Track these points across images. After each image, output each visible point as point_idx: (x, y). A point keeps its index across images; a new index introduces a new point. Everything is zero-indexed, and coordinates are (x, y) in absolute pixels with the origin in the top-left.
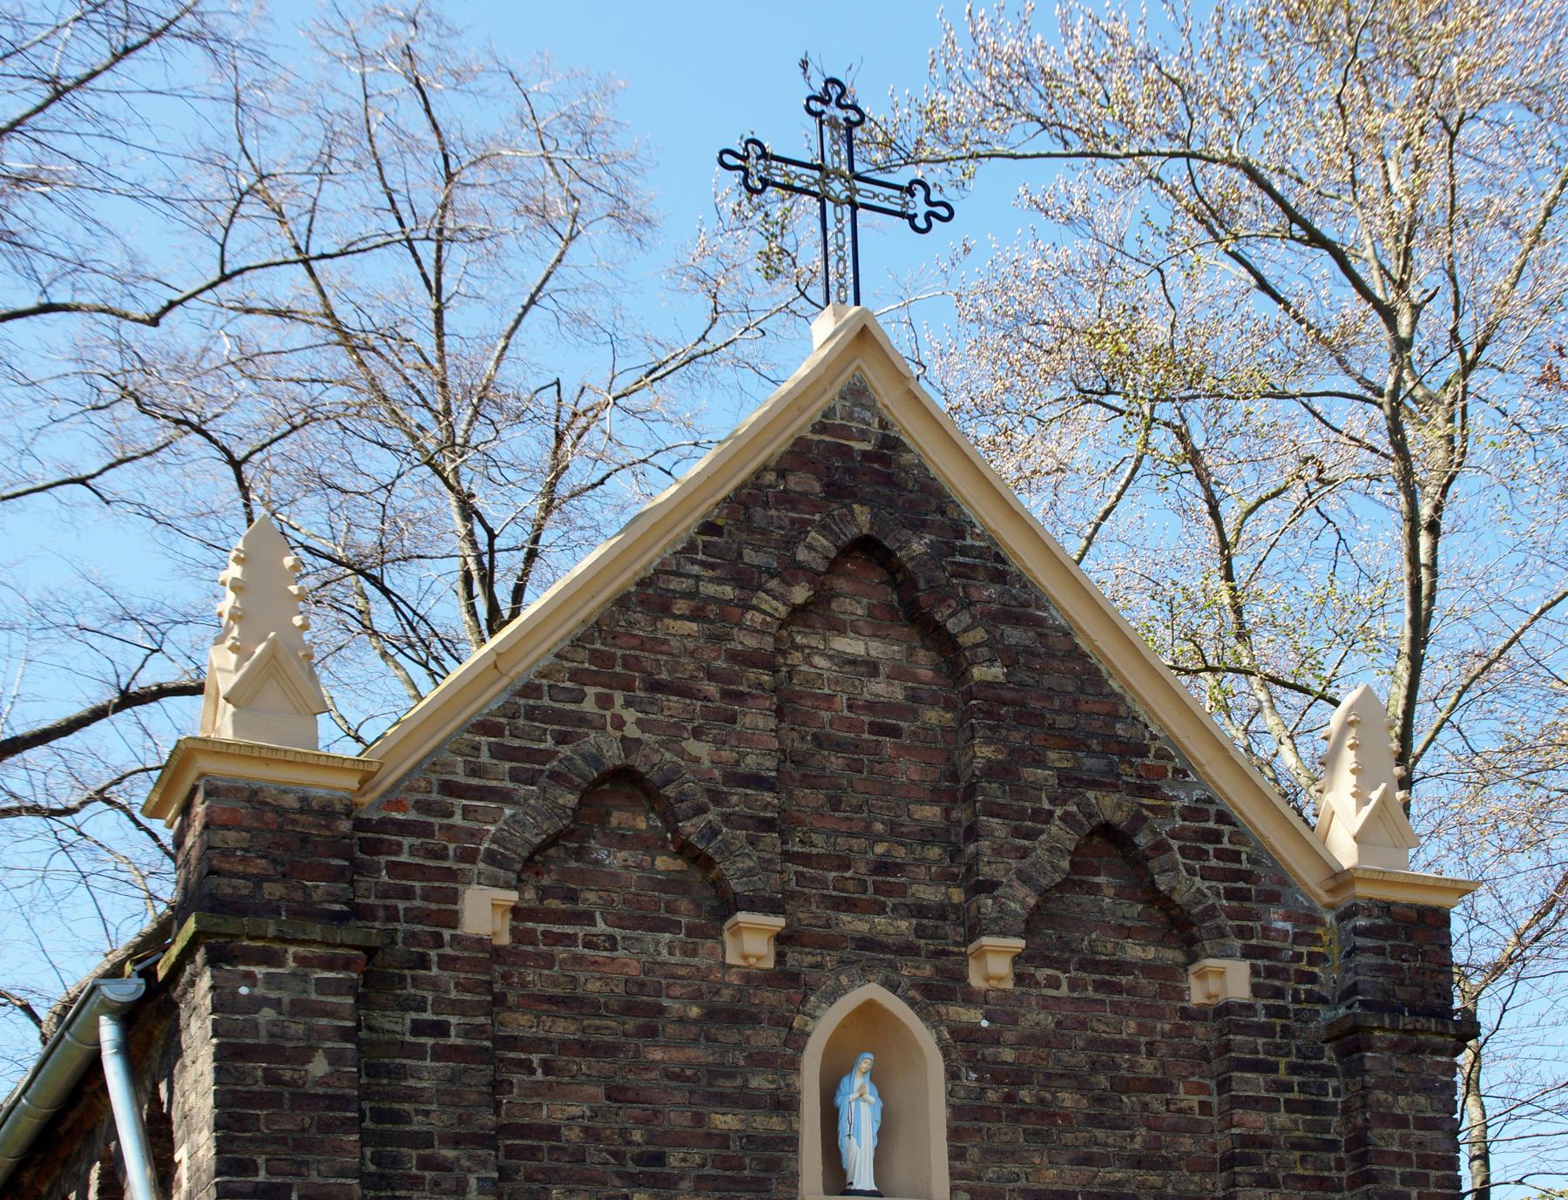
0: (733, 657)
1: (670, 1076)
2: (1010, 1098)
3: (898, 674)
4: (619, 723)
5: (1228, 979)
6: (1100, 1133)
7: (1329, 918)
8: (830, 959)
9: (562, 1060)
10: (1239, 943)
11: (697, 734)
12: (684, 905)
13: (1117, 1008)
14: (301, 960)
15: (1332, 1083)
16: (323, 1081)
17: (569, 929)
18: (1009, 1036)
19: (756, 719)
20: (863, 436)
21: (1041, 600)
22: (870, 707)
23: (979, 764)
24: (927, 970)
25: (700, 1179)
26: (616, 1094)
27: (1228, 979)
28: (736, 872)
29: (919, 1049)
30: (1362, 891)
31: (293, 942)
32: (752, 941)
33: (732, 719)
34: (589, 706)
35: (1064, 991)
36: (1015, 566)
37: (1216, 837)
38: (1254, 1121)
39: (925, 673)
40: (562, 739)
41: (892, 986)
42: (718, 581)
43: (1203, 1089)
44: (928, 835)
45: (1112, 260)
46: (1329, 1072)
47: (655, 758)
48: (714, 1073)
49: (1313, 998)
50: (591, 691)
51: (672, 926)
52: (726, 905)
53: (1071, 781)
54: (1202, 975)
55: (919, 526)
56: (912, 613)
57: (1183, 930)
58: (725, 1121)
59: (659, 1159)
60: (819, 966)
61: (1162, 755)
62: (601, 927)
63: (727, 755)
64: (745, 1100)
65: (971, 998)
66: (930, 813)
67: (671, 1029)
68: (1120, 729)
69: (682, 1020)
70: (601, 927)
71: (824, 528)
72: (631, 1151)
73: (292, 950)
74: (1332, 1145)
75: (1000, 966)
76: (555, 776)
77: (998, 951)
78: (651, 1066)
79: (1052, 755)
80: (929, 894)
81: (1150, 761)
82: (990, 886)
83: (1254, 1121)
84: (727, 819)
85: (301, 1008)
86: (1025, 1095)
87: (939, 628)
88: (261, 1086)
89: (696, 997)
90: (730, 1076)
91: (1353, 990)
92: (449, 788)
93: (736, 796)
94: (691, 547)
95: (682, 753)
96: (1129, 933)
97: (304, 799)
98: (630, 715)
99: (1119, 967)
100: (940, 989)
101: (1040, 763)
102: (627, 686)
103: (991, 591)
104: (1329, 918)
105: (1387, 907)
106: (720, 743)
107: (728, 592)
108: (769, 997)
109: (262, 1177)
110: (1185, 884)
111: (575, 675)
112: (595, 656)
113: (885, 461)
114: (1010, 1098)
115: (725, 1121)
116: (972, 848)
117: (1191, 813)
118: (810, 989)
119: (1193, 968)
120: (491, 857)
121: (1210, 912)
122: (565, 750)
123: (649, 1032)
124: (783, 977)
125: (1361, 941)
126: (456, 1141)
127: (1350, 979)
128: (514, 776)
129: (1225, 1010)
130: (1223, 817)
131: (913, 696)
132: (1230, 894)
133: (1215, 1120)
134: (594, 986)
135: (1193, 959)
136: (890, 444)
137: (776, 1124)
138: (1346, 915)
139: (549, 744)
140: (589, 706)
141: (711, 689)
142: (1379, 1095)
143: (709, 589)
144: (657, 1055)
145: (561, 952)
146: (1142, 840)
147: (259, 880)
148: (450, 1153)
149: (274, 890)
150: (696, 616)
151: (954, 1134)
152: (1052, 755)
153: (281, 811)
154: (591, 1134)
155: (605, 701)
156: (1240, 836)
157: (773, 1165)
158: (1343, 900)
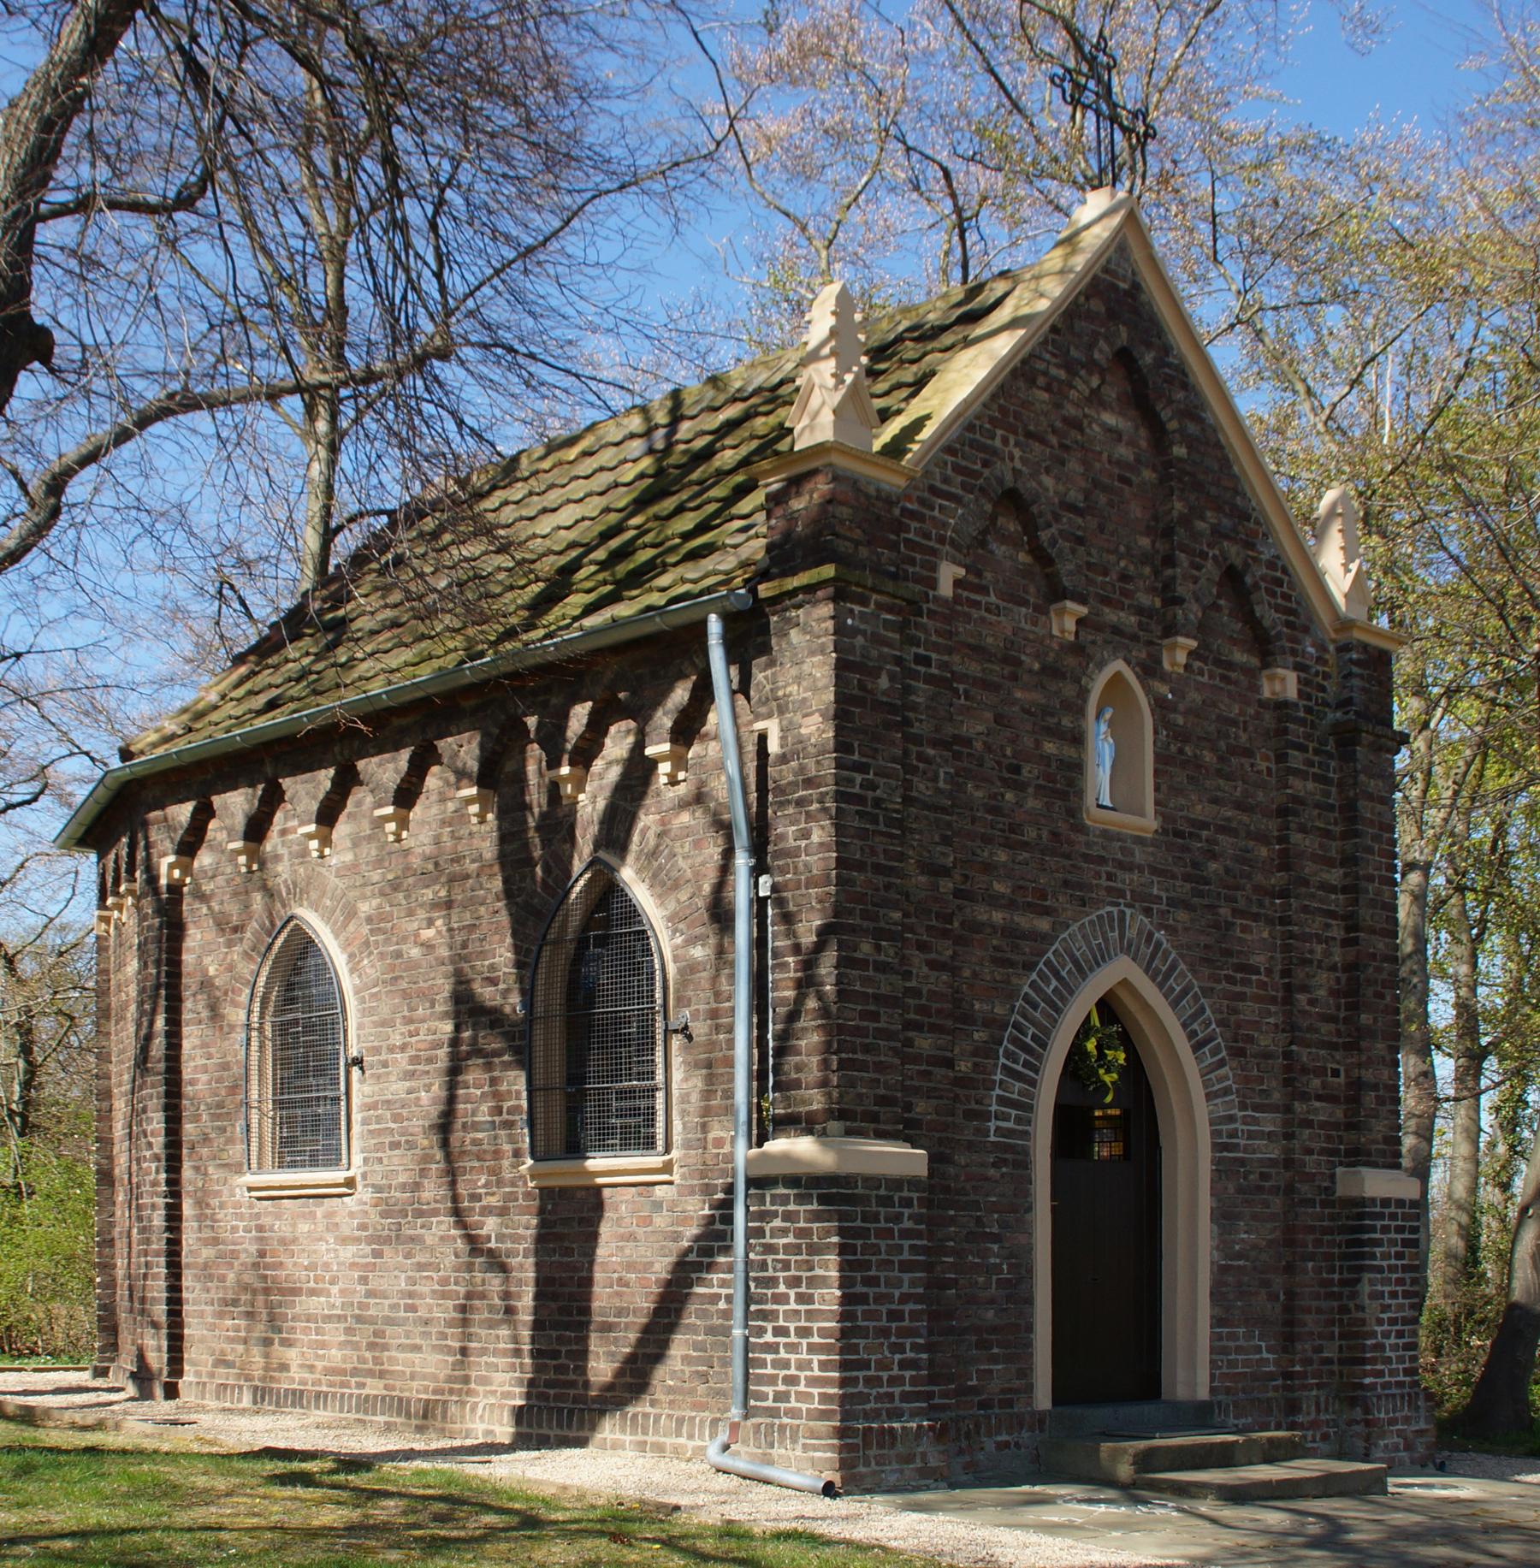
0: (1065, 420)
1: (1028, 712)
2: (1181, 751)
3: (1132, 443)
4: (1012, 458)
5: (1284, 684)
6: (1221, 782)
7: (1331, 648)
8: (1099, 639)
9: (973, 691)
10: (1291, 659)
11: (1048, 471)
12: (1032, 589)
13: (1230, 695)
14: (879, 606)
15: (1333, 764)
16: (884, 693)
17: (978, 597)
18: (1181, 707)
19: (1074, 466)
20: (1124, 280)
21: (1203, 405)
22: (1119, 463)
23: (1175, 514)
24: (1143, 655)
25: (1038, 787)
26: (998, 719)
27: (1284, 684)
28: (1066, 569)
29: (1139, 709)
30: (1357, 635)
31: (880, 592)
32: (1066, 620)
33: (1063, 464)
34: (998, 443)
35: (1205, 679)
36: (1191, 379)
37: (1279, 583)
38: (1298, 786)
39: (1143, 444)
40: (986, 464)
41: (1128, 663)
42: (1058, 366)
43: (1267, 759)
44: (1146, 559)
45: (1412, 246)
46: (1330, 756)
47: (1028, 486)
48: (1047, 712)
49: (1326, 704)
50: (999, 432)
51: (1025, 603)
52: (1056, 593)
53: (1217, 533)
54: (1271, 678)
55: (1149, 346)
56: (1141, 402)
57: (1264, 647)
58: (1050, 747)
59: (1016, 770)
60: (1093, 642)
61: (1257, 523)
62: (993, 599)
63: (1061, 488)
64: (1056, 733)
65: (1164, 677)
66: (1145, 542)
67: (1026, 677)
68: (1238, 500)
69: (1030, 671)
70: (993, 599)
71: (1107, 339)
72: (1006, 762)
73: (874, 596)
74: (1331, 808)
75: (1181, 657)
76: (982, 489)
77: (1072, 613)
78: (1015, 702)
79: (1209, 514)
80: (1145, 599)
81: (1252, 525)
82: (1179, 601)
83: (1298, 786)
84: (1061, 532)
85: (877, 640)
86: (1188, 750)
87: (1156, 415)
88: (856, 692)
89: (1037, 656)
90: (1052, 715)
91: (1348, 702)
92: (933, 490)
93: (1067, 516)
94: (1045, 342)
95: (1040, 483)
96: (1234, 642)
97: (878, 490)
98: (1017, 453)
99: (1230, 665)
100: (1149, 670)
101: (1203, 518)
102: (1015, 433)
103: (1180, 395)
104: (1331, 648)
105: (1365, 647)
106: (1058, 479)
107: (1062, 374)
108: (1071, 661)
109: (856, 757)
110: (1268, 616)
111: (992, 420)
112: (1002, 409)
113: (1135, 299)
114: (1181, 751)
115: (1050, 747)
116: (1169, 572)
117: (1271, 565)
118: (1090, 658)
119: (1265, 672)
120: (953, 543)
121: (1279, 636)
122: (986, 472)
123: (1014, 677)
124: (1077, 649)
125: (1355, 669)
126: (935, 744)
127: (1346, 694)
128: (964, 486)
129: (1281, 706)
130: (1285, 571)
131: (1138, 460)
132: (1288, 624)
133: (1273, 780)
134: (990, 640)
135: (1266, 665)
136: (1136, 287)
137: (1069, 752)
138: (1344, 648)
139: (978, 467)
140: (998, 443)
141: (1054, 440)
142: (1362, 777)
143: (1054, 371)
144: (1018, 695)
145: (975, 614)
146: (1248, 580)
147: (857, 543)
148: (931, 752)
149: (864, 552)
150: (1048, 389)
151: (1156, 772)
152: (1209, 514)
153: (867, 496)
154: (988, 747)
155: (1005, 441)
156: (1291, 586)
157: (1071, 783)
158: (1342, 638)
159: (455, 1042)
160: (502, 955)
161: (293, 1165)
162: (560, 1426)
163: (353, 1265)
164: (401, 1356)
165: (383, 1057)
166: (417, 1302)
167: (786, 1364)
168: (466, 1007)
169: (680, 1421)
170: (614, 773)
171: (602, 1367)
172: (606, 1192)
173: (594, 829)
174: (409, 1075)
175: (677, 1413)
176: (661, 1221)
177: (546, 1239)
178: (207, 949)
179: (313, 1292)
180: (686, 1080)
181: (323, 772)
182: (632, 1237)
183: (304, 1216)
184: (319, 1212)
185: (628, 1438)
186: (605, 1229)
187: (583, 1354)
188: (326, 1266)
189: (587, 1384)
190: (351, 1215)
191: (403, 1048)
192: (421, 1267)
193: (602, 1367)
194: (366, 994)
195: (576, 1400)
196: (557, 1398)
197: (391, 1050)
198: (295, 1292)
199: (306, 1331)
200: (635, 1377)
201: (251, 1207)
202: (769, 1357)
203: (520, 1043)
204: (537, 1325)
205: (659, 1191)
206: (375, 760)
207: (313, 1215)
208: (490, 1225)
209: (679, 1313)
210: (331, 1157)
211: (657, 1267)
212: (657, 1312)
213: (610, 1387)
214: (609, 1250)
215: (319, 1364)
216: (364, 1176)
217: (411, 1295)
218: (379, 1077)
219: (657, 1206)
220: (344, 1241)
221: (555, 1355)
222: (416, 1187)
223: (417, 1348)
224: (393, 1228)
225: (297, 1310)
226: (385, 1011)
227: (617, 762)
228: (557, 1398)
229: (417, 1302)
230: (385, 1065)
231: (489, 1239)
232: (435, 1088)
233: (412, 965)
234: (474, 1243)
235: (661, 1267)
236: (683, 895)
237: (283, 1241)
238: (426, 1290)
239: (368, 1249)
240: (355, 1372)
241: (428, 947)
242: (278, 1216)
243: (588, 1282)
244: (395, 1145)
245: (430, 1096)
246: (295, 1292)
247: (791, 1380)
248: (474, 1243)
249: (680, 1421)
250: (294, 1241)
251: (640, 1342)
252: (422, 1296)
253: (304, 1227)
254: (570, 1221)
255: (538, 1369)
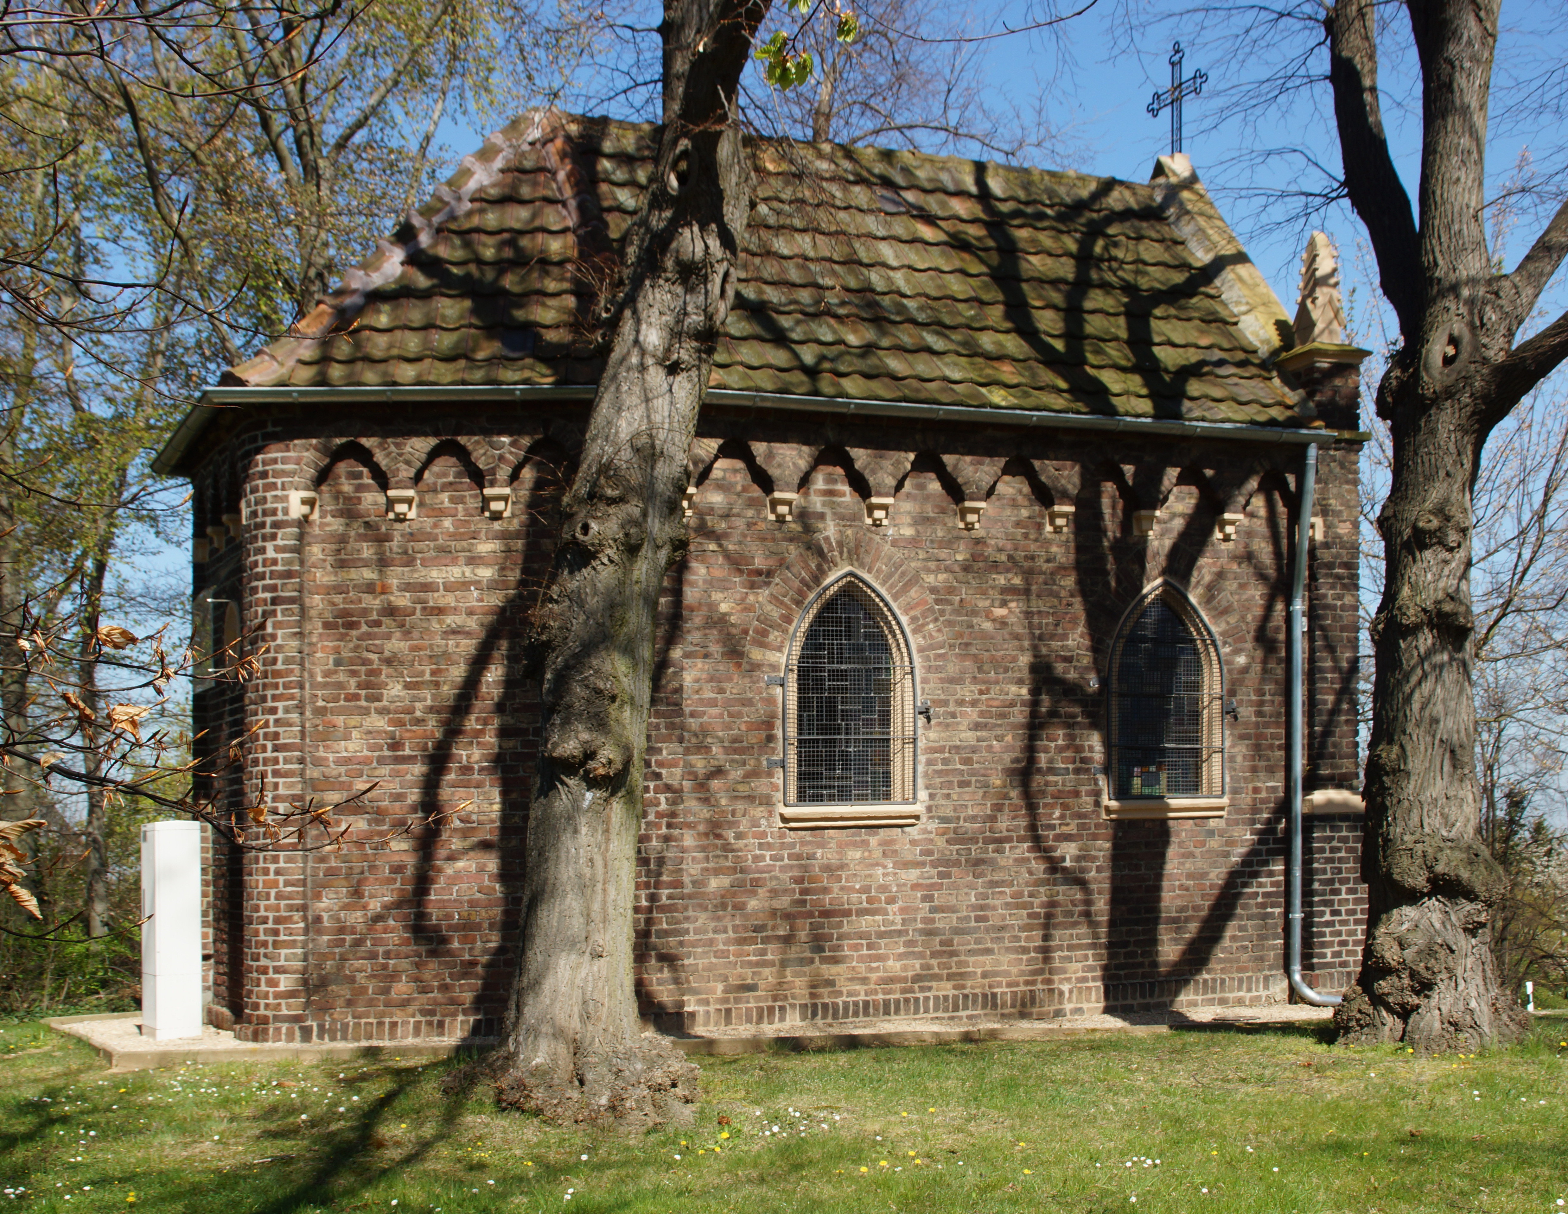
159: (1034, 704)
160: (1076, 639)
161: (817, 799)
162: (1143, 996)
163: (915, 887)
164: (971, 959)
165: (951, 708)
166: (989, 913)
167: (1339, 933)
168: (1043, 676)
169: (1241, 980)
170: (1178, 524)
171: (1169, 950)
172: (1171, 823)
173: (1162, 561)
174: (977, 727)
175: (1245, 975)
176: (1214, 843)
177: (1118, 856)
178: (712, 583)
179: (861, 912)
180: (1233, 746)
181: (1076, 480)
182: (1192, 855)
183: (855, 845)
184: (873, 841)
185: (1199, 998)
186: (1172, 852)
187: (1153, 941)
188: (883, 889)
189: (1155, 964)
190: (913, 842)
191: (974, 703)
192: (993, 884)
193: (1169, 950)
194: (931, 654)
195: (1144, 976)
196: (1127, 976)
197: (961, 703)
198: (847, 913)
199: (856, 948)
200: (1197, 956)
201: (782, 836)
202: (1327, 930)
203: (1095, 712)
204: (1112, 923)
205: (1212, 823)
206: (968, 459)
207: (865, 843)
208: (1068, 851)
209: (1233, 907)
210: (881, 790)
211: (1212, 875)
212: (1214, 908)
213: (1176, 964)
214: (1177, 867)
215: (874, 976)
216: (929, 809)
217: (982, 908)
218: (947, 725)
219: (1211, 833)
220: (907, 865)
221: (1125, 944)
222: (993, 819)
223: (988, 951)
224: (967, 851)
225: (846, 928)
226: (952, 668)
227: (1182, 515)
228: (1127, 976)
229: (989, 913)
230: (953, 715)
231: (1063, 859)
232: (1009, 738)
233: (984, 635)
234: (1054, 866)
235: (1217, 876)
236: (1233, 619)
237: (827, 868)
238: (997, 902)
239: (934, 872)
240: (917, 979)
241: (1003, 623)
242: (822, 845)
243: (1158, 889)
244: (963, 784)
245: (1006, 746)
246: (847, 913)
247: (1343, 943)
248: (1054, 866)
249: (1241, 980)
250: (842, 867)
251: (1201, 930)
252: (994, 908)
253: (854, 854)
254: (1140, 846)
255: (1111, 956)
